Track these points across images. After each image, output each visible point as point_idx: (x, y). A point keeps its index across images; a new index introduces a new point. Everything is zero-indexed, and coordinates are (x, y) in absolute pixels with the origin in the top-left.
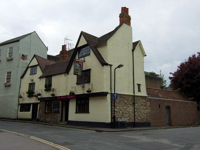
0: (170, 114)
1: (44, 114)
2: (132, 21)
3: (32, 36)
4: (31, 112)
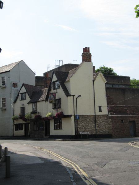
0: (135, 127)
1: (33, 131)
2: (137, 18)
3: (21, 65)
4: (23, 131)
